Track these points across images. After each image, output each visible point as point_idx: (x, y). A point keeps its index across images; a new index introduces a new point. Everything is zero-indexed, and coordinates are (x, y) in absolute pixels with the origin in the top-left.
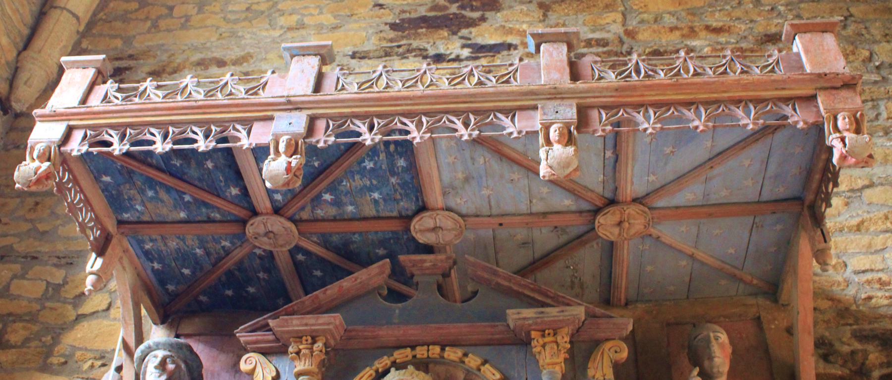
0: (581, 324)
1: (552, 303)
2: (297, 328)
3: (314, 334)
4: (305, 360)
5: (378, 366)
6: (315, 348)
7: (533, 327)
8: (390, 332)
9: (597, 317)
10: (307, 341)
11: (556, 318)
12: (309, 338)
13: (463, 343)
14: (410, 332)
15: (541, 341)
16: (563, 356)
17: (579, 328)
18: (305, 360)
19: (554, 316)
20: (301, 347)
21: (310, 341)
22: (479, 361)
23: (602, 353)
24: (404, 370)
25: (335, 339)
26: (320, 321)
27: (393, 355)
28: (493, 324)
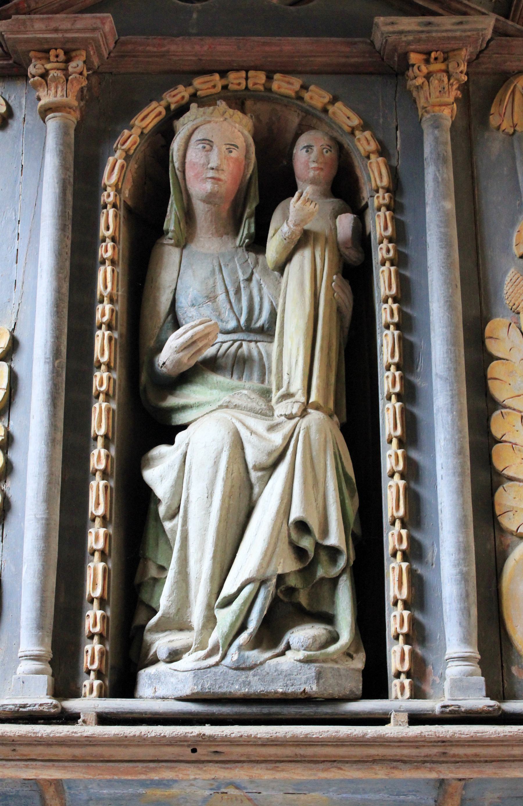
0: (484, 45)
1: (440, 11)
2: (41, 36)
3: (68, 46)
4: (56, 88)
5: (170, 100)
6: (70, 69)
7: (412, 47)
8: (188, 48)
9: (507, 35)
10: (57, 56)
11: (450, 34)
12: (61, 52)
13: (300, 69)
14: (220, 48)
15: (424, 69)
16: (454, 93)
17: (481, 52)
18: (56, 88)
19: (447, 31)
20: (48, 66)
21: (62, 57)
22: (327, 97)
23: (513, 92)
24: (212, 108)
25: (100, 56)
26: (79, 25)
27: (190, 84)
28: (350, 39)
